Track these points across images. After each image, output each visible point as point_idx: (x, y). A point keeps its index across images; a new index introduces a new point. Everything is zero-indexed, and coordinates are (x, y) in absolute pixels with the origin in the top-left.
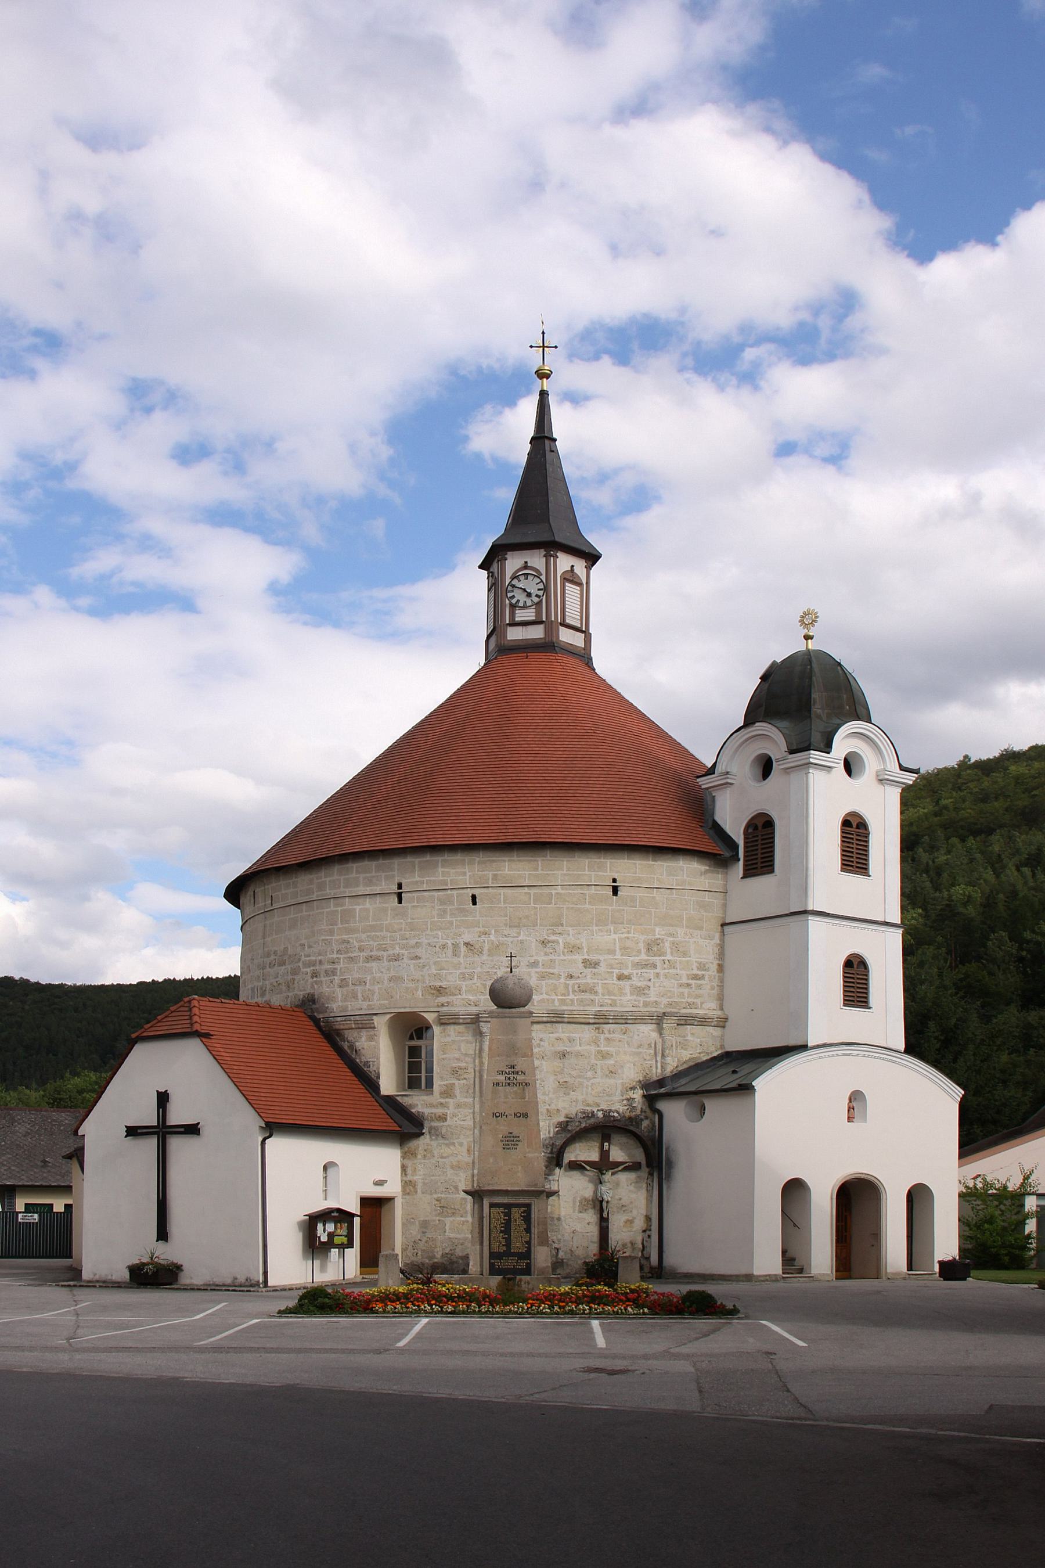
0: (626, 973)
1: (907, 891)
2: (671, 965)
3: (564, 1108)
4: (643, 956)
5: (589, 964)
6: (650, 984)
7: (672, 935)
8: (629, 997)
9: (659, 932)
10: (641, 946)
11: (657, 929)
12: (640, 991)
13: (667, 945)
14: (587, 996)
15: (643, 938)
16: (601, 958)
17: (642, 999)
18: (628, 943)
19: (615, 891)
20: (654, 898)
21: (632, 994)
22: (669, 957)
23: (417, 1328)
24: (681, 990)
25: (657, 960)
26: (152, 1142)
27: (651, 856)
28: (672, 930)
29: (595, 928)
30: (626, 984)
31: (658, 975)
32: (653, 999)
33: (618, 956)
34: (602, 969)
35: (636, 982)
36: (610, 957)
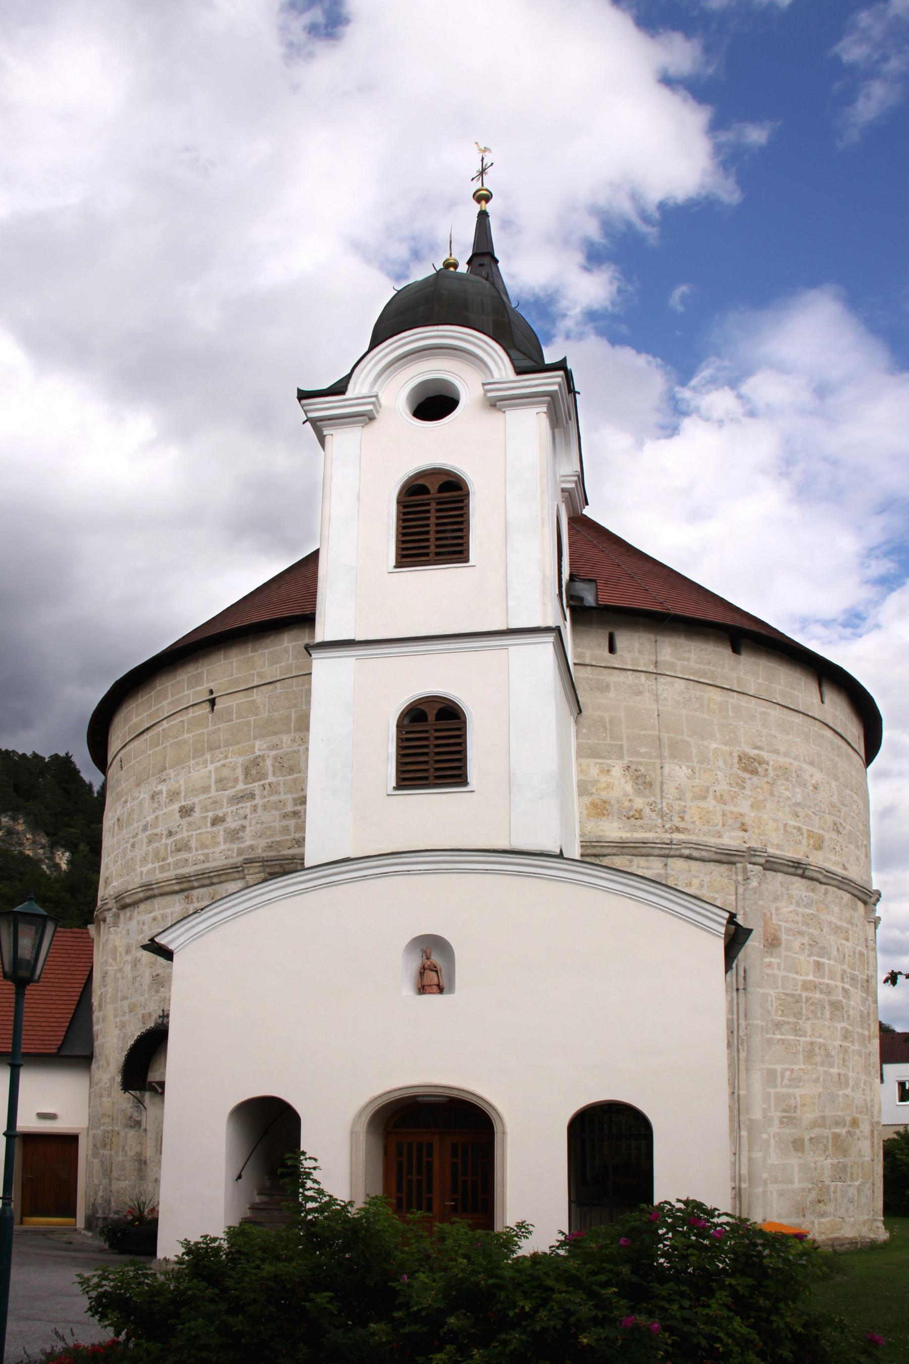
0: (221, 814)
1: (572, 1199)
2: (273, 789)
3: (154, 1011)
4: (241, 786)
5: (186, 812)
6: (246, 823)
7: (275, 747)
8: (223, 847)
9: (260, 746)
10: (239, 772)
11: (258, 744)
12: (234, 835)
13: (269, 762)
14: (183, 855)
15: (240, 760)
16: (196, 800)
17: (235, 846)
18: (226, 773)
19: (212, 702)
20: (253, 702)
21: (225, 842)
22: (271, 779)
23: (789, 1037)
24: (285, 823)
25: (256, 786)
26: (26, 1047)
27: (250, 646)
28: (275, 739)
29: (192, 762)
30: (220, 829)
31: (255, 809)
32: (248, 843)
33: (213, 793)
34: (197, 814)
35: (232, 824)
36: (205, 796)
